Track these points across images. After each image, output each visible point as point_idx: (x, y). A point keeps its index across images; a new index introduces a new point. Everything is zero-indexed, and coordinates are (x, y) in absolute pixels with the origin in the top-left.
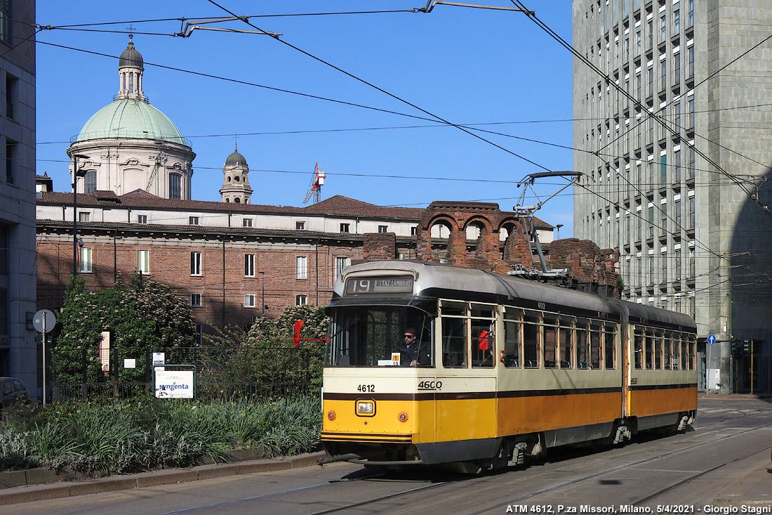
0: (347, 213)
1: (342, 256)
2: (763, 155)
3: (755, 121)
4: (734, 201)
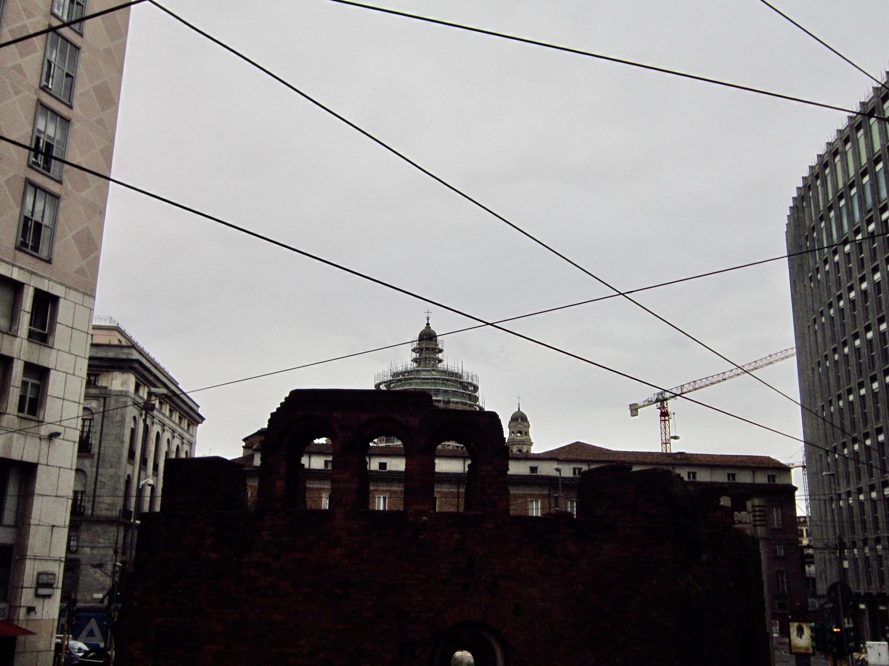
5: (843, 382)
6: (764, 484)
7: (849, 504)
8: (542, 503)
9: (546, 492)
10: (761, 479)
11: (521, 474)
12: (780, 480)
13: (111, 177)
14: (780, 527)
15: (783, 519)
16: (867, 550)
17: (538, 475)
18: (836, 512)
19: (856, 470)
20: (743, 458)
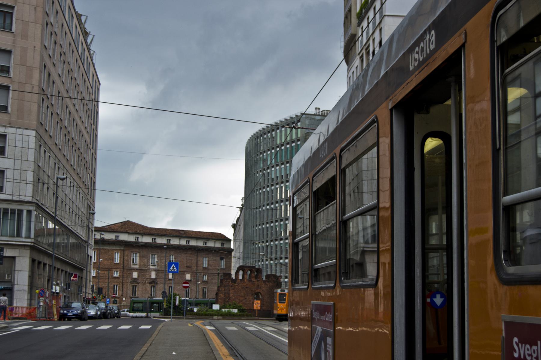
6: (219, 247)
9: (122, 248)
10: (218, 245)
12: (226, 246)
13: (37, 94)
14: (224, 268)
15: (226, 265)
16: (260, 209)
18: (254, 231)
20: (210, 234)
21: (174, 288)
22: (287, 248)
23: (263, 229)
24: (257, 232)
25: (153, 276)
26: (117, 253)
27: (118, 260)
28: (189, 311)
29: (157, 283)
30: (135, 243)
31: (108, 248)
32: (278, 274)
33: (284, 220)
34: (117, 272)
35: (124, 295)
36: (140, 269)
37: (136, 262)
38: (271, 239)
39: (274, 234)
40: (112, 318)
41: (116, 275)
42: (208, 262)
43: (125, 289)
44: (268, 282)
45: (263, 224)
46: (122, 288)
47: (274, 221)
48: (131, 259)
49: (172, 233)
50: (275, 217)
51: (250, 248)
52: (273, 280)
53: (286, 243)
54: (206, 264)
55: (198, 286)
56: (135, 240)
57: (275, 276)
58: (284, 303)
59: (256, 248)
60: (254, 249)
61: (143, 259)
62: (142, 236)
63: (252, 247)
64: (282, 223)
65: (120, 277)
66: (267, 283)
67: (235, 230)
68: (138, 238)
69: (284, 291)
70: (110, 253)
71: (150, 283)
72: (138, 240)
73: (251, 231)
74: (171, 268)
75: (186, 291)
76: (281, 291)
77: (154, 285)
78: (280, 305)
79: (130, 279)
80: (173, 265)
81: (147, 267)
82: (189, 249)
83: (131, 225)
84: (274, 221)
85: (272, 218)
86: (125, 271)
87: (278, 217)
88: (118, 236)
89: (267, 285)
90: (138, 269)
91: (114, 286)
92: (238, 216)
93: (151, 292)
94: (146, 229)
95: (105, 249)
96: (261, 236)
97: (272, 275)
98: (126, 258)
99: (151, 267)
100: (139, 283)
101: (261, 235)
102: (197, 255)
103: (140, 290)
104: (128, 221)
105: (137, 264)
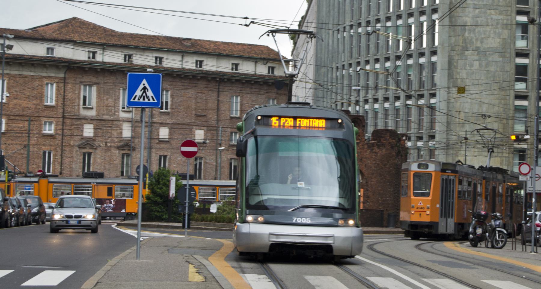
0: (101, 42)
1: (89, 83)
2: (492, 32)
3: (487, 3)
4: (469, 68)
5: (373, 11)
7: (349, 73)
8: (58, 87)
10: (262, 70)
11: (30, 54)
17: (54, 57)
18: (340, 41)
19: (359, 8)
20: (245, 47)
21: (170, 158)
22: (409, 75)
23: (360, 36)
24: (346, 42)
25: (127, 132)
26: (49, 85)
27: (51, 99)
28: (198, 210)
29: (134, 149)
30: (90, 63)
31: (32, 74)
32: (400, 131)
33: (404, 16)
34: (51, 123)
35: (64, 172)
36: (99, 118)
37: (90, 104)
38: (376, 57)
39: (382, 47)
40: (22, 225)
41: (49, 129)
42: (241, 108)
43: (66, 161)
44: (379, 146)
45: (359, 25)
46: (62, 158)
47: (383, 18)
48: (79, 98)
49: (166, 44)
50: (386, 11)
51: (330, 76)
52: (390, 143)
53: (409, 66)
54: (236, 110)
55: (221, 155)
56: (89, 58)
57: (393, 133)
58: (428, 195)
59: (343, 76)
60: (339, 77)
61: (105, 98)
62: (104, 49)
63: (334, 75)
64: (400, 22)
65: (57, 134)
66: (376, 149)
67: (295, 44)
68: (94, 53)
69: (427, 167)
70: (36, 84)
71: (120, 148)
72: (94, 57)
73: (333, 41)
74: (138, 93)
75: (196, 165)
76: (419, 166)
77: (129, 152)
78: (417, 201)
79: (77, 138)
80: (144, 81)
81: (114, 114)
82: (202, 77)
83: (79, 27)
84: (383, 18)
85: (379, 12)
86: (68, 121)
87: (391, 10)
88: (52, 49)
89: (377, 153)
90: (96, 118)
91: (44, 153)
92: (303, 14)
93: (123, 168)
94: (112, 35)
95: (25, 77)
96: (355, 50)
97: (387, 131)
98: (69, 95)
99: (123, 115)
100: (96, 149)
101: (354, 49)
102: (218, 91)
103: (99, 161)
104: (74, 19)
105: (92, 108)
